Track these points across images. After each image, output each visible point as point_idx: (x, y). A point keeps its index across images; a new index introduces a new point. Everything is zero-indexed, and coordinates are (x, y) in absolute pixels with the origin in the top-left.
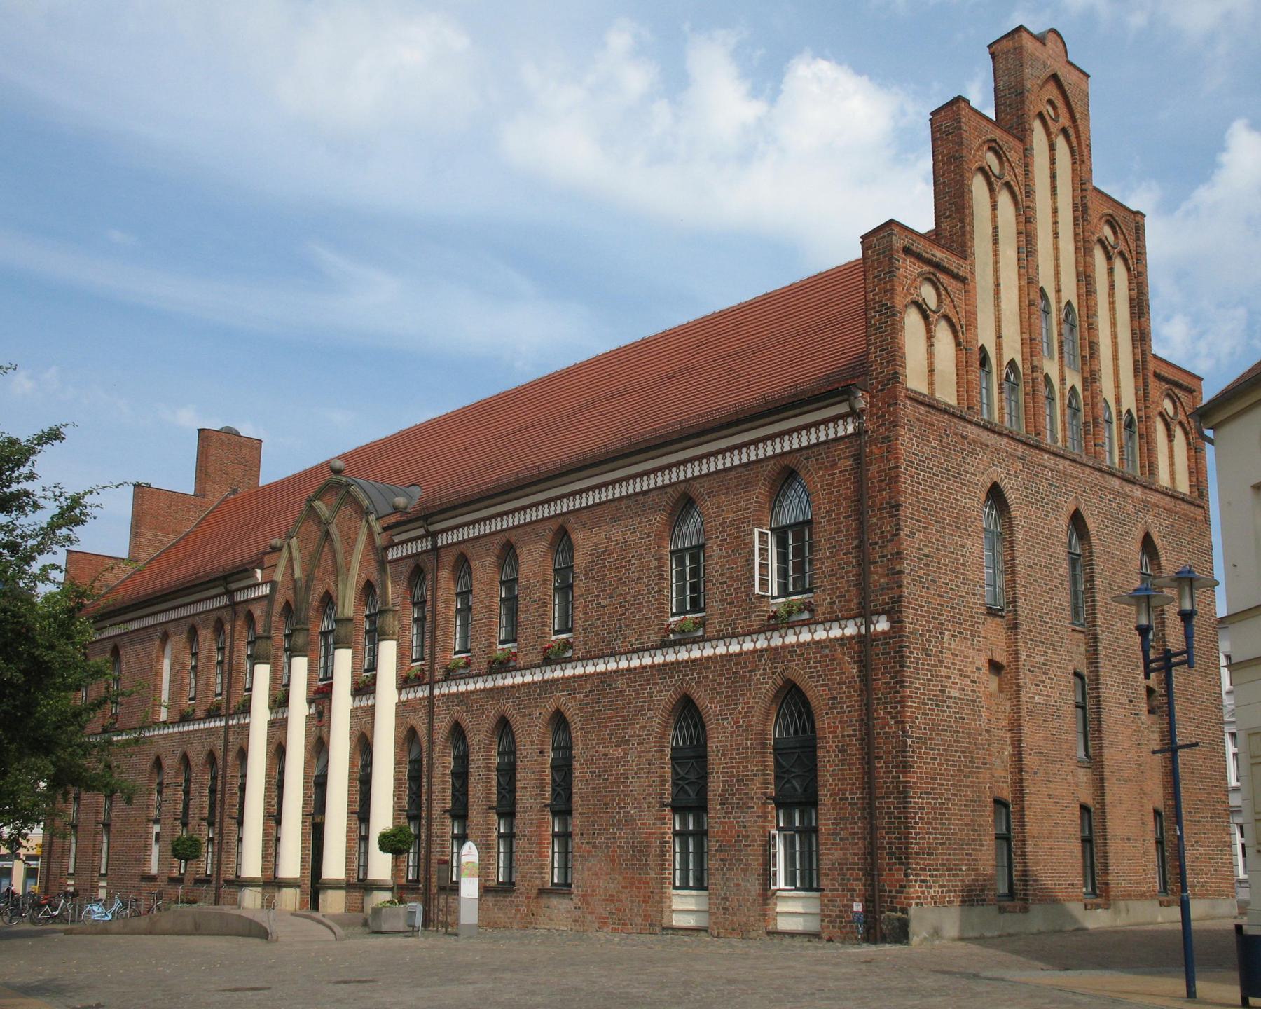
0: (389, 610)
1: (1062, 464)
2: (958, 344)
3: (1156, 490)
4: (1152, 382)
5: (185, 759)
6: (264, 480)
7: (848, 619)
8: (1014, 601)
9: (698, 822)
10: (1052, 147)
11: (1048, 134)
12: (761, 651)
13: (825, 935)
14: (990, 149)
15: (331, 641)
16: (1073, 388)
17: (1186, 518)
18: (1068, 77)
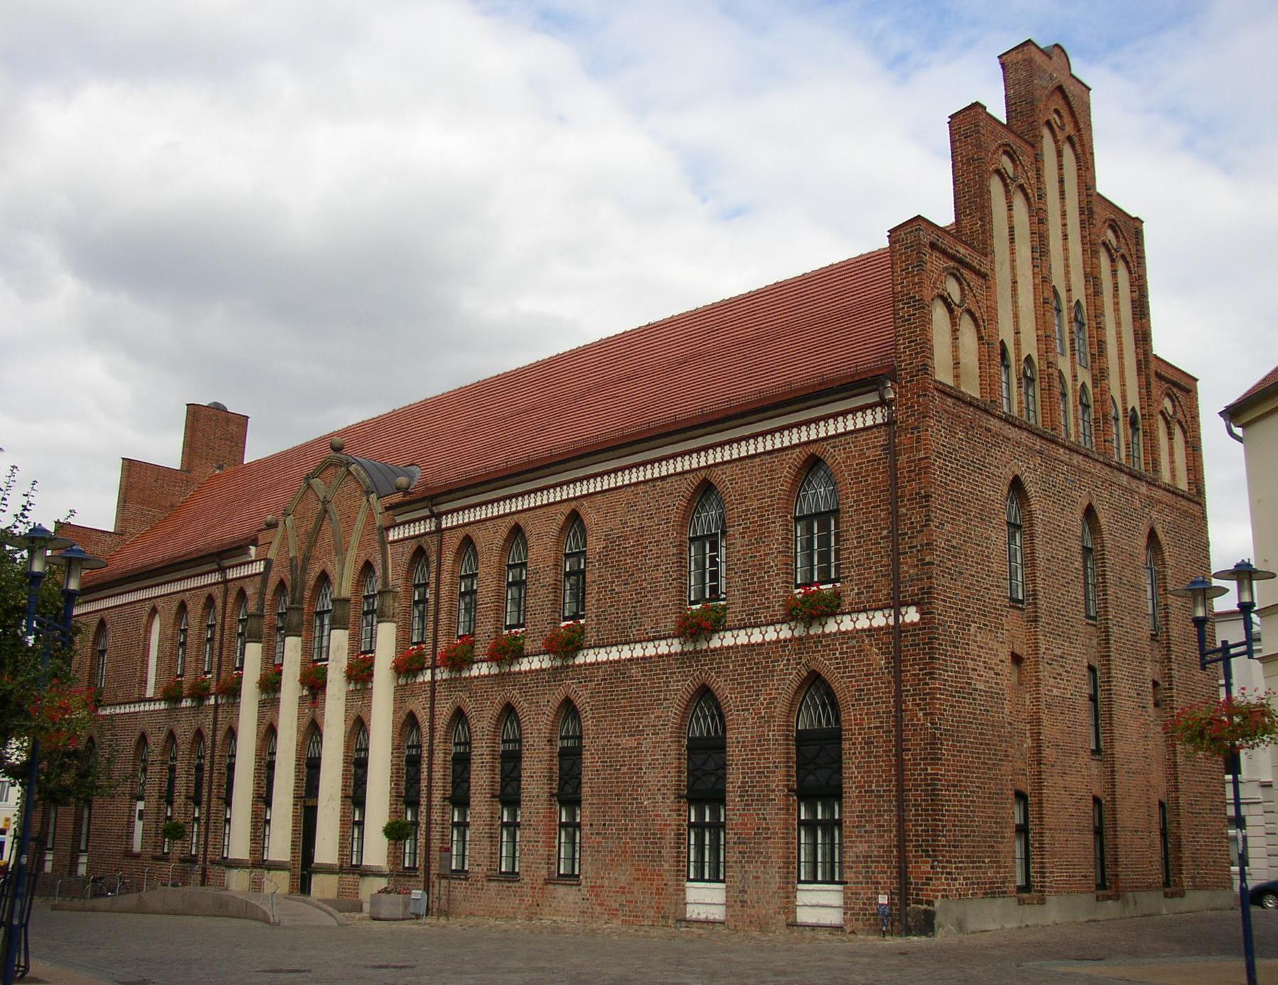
0: (390, 591)
1: (1077, 459)
2: (980, 338)
3: (1159, 487)
4: (1153, 379)
5: (171, 736)
6: (248, 459)
7: (876, 610)
8: (1034, 594)
9: (715, 814)
10: (1059, 154)
11: (1056, 141)
12: (785, 640)
13: (848, 929)
14: (1005, 152)
15: (327, 621)
16: (1083, 385)
17: (1185, 514)
18: (1071, 88)
